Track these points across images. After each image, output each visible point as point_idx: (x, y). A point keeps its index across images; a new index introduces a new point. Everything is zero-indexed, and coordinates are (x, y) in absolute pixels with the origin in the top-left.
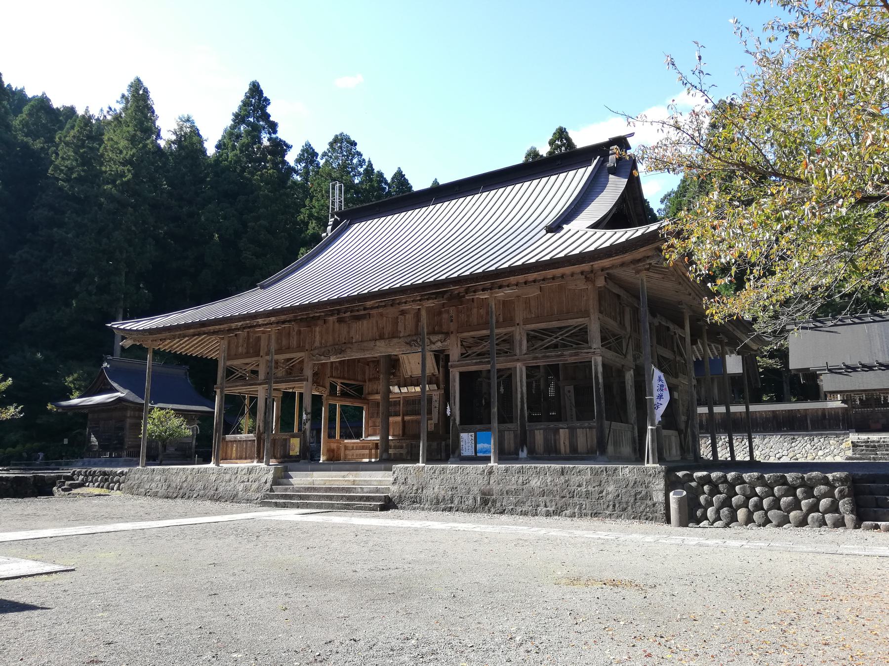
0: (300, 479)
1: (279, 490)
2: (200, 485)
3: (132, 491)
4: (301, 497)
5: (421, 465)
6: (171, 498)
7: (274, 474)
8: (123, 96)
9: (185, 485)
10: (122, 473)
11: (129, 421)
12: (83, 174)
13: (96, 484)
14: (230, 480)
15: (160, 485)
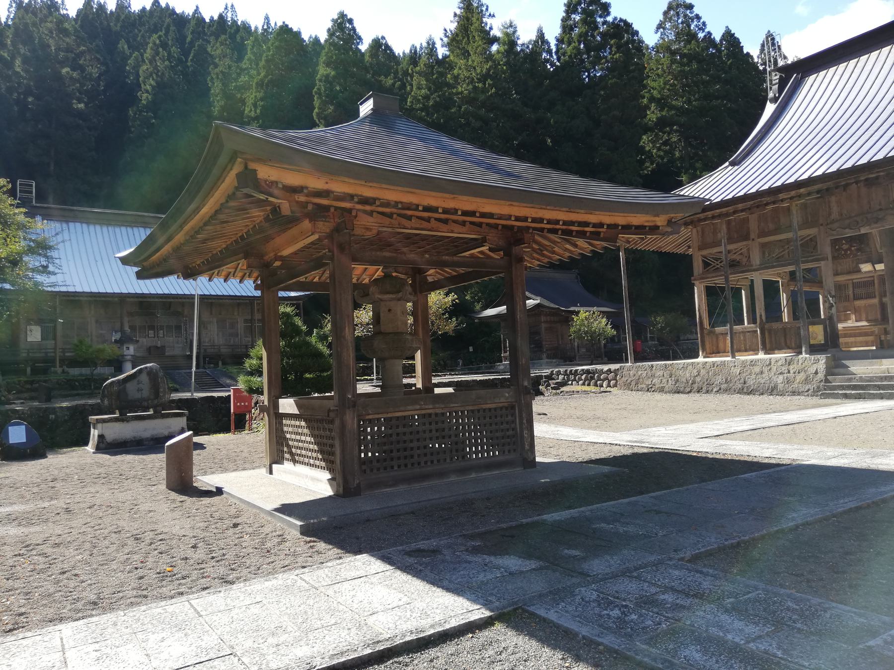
0: (860, 369)
1: (837, 381)
2: (719, 379)
3: (628, 386)
4: (879, 387)
5: (804, 355)
6: (683, 392)
7: (826, 363)
8: (455, 15)
9: (698, 379)
10: (609, 371)
11: (543, 326)
12: (438, 99)
13: (581, 382)
14: (762, 373)
15: (664, 381)
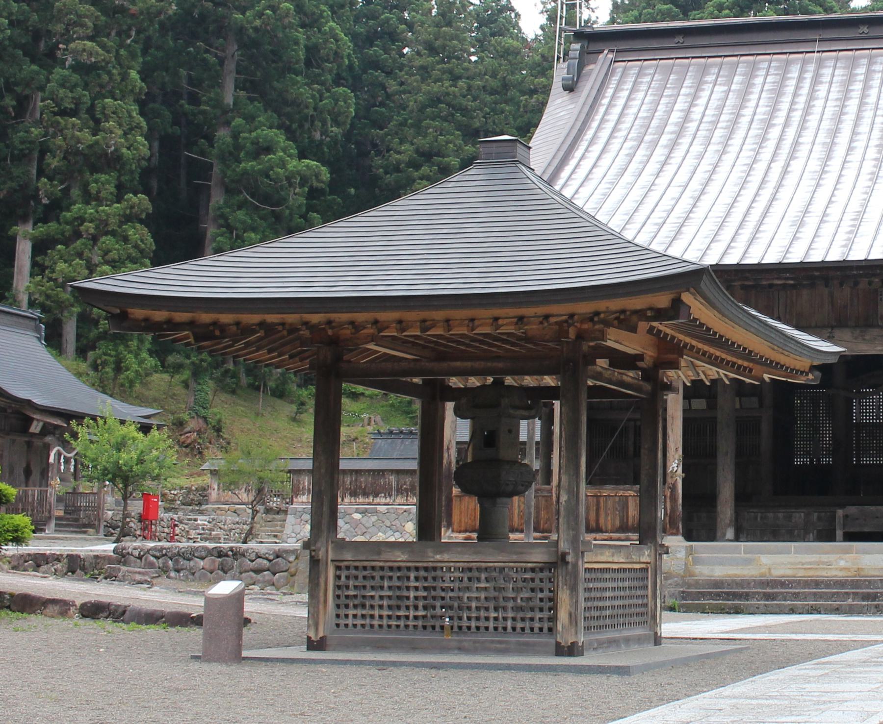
4: (768, 597)
